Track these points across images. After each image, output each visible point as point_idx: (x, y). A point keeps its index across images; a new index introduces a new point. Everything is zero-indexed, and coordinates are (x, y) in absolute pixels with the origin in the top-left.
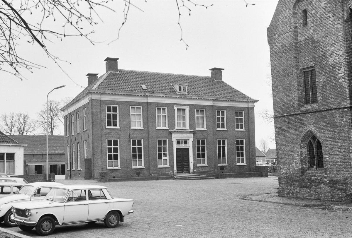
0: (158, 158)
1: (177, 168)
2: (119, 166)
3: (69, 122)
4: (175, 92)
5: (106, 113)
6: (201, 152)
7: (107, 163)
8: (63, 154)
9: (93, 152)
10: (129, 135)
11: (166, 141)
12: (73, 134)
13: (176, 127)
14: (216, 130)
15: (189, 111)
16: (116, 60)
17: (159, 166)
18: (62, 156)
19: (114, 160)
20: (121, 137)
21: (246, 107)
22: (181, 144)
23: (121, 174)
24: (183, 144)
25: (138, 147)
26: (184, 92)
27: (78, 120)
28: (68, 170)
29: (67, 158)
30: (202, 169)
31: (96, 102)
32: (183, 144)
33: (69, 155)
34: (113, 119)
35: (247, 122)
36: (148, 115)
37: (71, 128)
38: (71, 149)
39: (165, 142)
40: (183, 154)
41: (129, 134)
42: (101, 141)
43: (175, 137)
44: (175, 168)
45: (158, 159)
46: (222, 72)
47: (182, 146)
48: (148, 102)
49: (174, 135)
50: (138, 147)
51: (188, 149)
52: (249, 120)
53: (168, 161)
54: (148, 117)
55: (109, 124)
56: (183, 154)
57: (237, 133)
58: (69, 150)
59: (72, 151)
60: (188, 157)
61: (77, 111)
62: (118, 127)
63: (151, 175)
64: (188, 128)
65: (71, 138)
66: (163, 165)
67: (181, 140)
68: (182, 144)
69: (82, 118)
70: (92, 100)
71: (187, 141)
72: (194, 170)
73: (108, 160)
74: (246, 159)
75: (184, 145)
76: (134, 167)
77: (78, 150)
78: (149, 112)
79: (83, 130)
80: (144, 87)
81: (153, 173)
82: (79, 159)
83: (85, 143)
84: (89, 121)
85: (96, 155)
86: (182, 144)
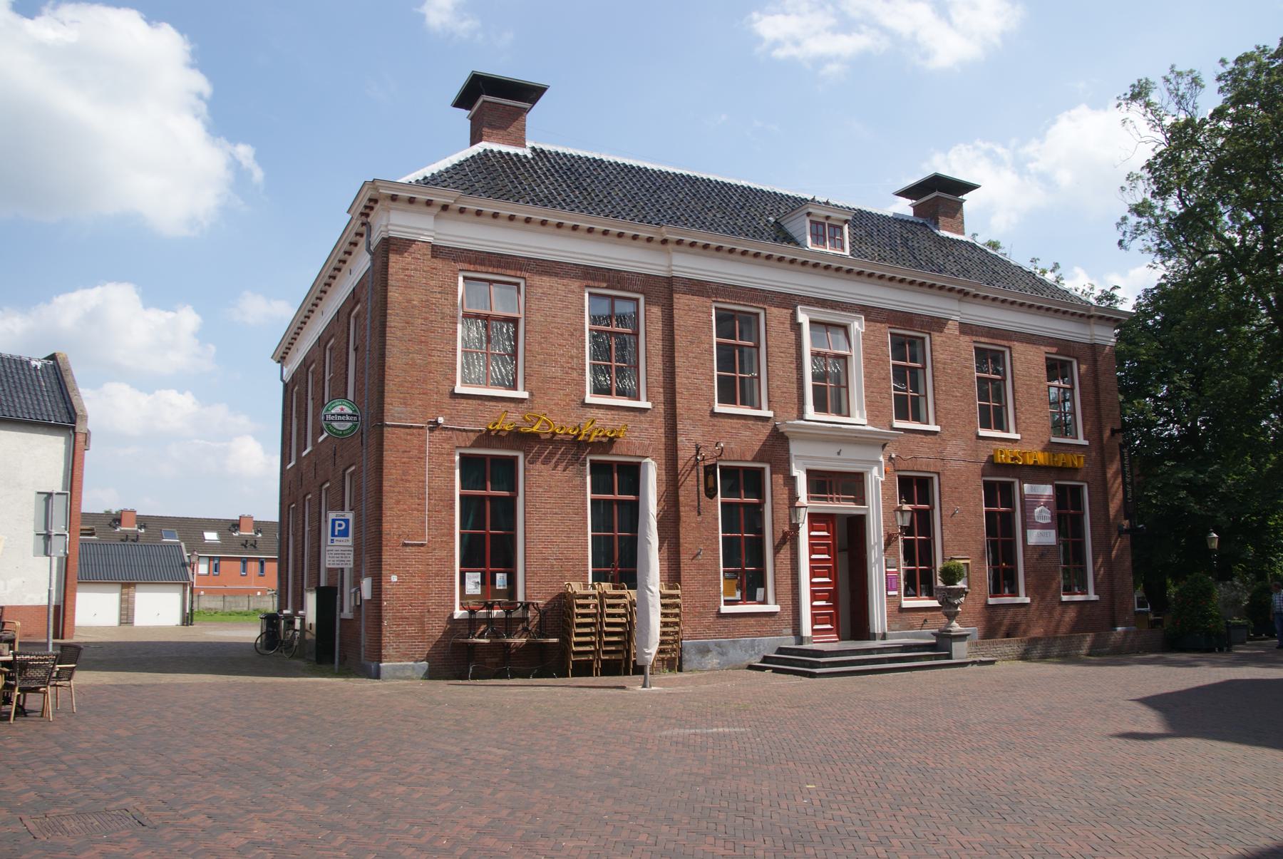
13: (810, 412)
46: (961, 203)
52: (1098, 402)
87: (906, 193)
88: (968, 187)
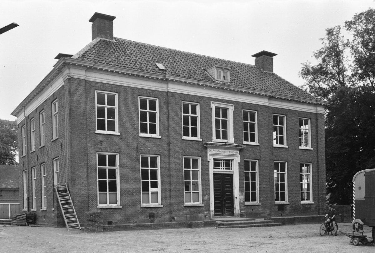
0: (185, 191)
1: (215, 207)
2: (119, 203)
3: (27, 131)
4: (211, 80)
5: (96, 105)
6: (250, 182)
7: (97, 197)
8: (17, 190)
9: (71, 176)
10: (137, 148)
11: (197, 160)
12: (33, 150)
13: (214, 139)
14: (272, 146)
15: (234, 113)
16: (111, 19)
17: (187, 204)
18: (16, 193)
19: (109, 191)
20: (122, 151)
21: (314, 113)
22: (220, 167)
23: (122, 216)
24: (224, 168)
25: (151, 170)
26: (224, 81)
27: (41, 124)
28: (42, 211)
29: (23, 191)
30: (253, 210)
31: (78, 84)
32: (223, 167)
33: (27, 187)
34: (108, 118)
35: (314, 137)
36: (168, 115)
37: (29, 141)
38: (30, 175)
39: (195, 162)
40: (223, 183)
41: (135, 145)
42: (87, 156)
43: (212, 155)
44: (212, 208)
45: (185, 192)
46: (273, 59)
47: (222, 170)
48: (169, 91)
49: (211, 151)
50: (151, 170)
51: (231, 176)
52: (317, 134)
53: (201, 197)
54: (168, 117)
55: (101, 126)
56: (223, 183)
57: (301, 153)
58: (26, 179)
59: (31, 179)
60: (230, 189)
61: (40, 109)
62: (117, 132)
63: (173, 218)
64: (231, 139)
65: (30, 157)
66: (192, 201)
67: (221, 161)
68: (222, 168)
69: (51, 119)
70: (70, 80)
71: (214, 167)
72: (240, 211)
73: (98, 192)
74: (313, 194)
75: (226, 169)
76: (144, 205)
77: (43, 175)
78: (170, 108)
79: (52, 138)
80: (161, 66)
81: (176, 215)
82: (43, 192)
83: (54, 162)
84: (63, 121)
85: (77, 181)
86: (222, 168)
87: (254, 56)
88: (275, 55)
